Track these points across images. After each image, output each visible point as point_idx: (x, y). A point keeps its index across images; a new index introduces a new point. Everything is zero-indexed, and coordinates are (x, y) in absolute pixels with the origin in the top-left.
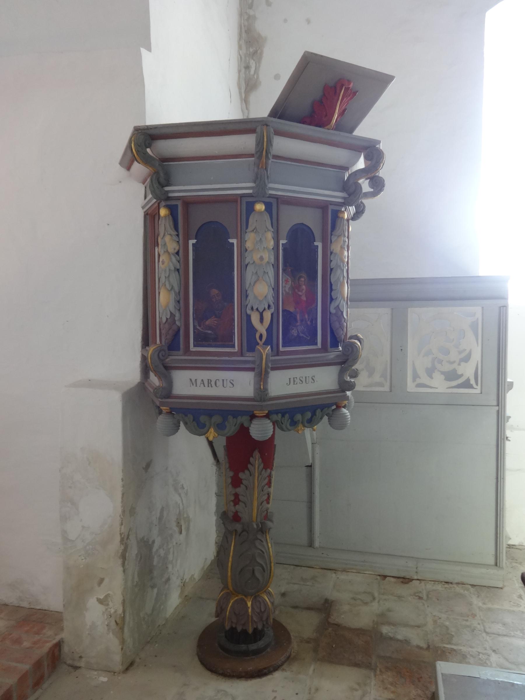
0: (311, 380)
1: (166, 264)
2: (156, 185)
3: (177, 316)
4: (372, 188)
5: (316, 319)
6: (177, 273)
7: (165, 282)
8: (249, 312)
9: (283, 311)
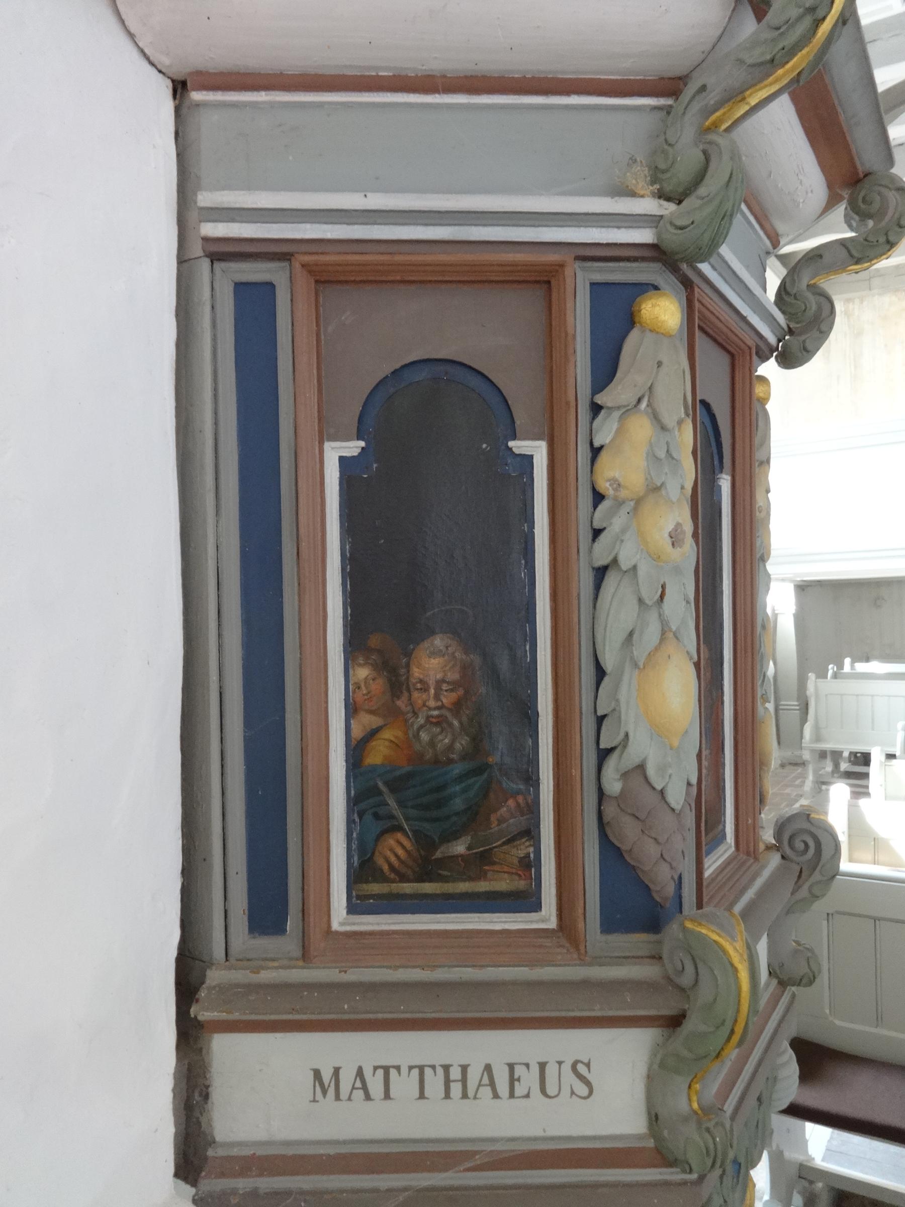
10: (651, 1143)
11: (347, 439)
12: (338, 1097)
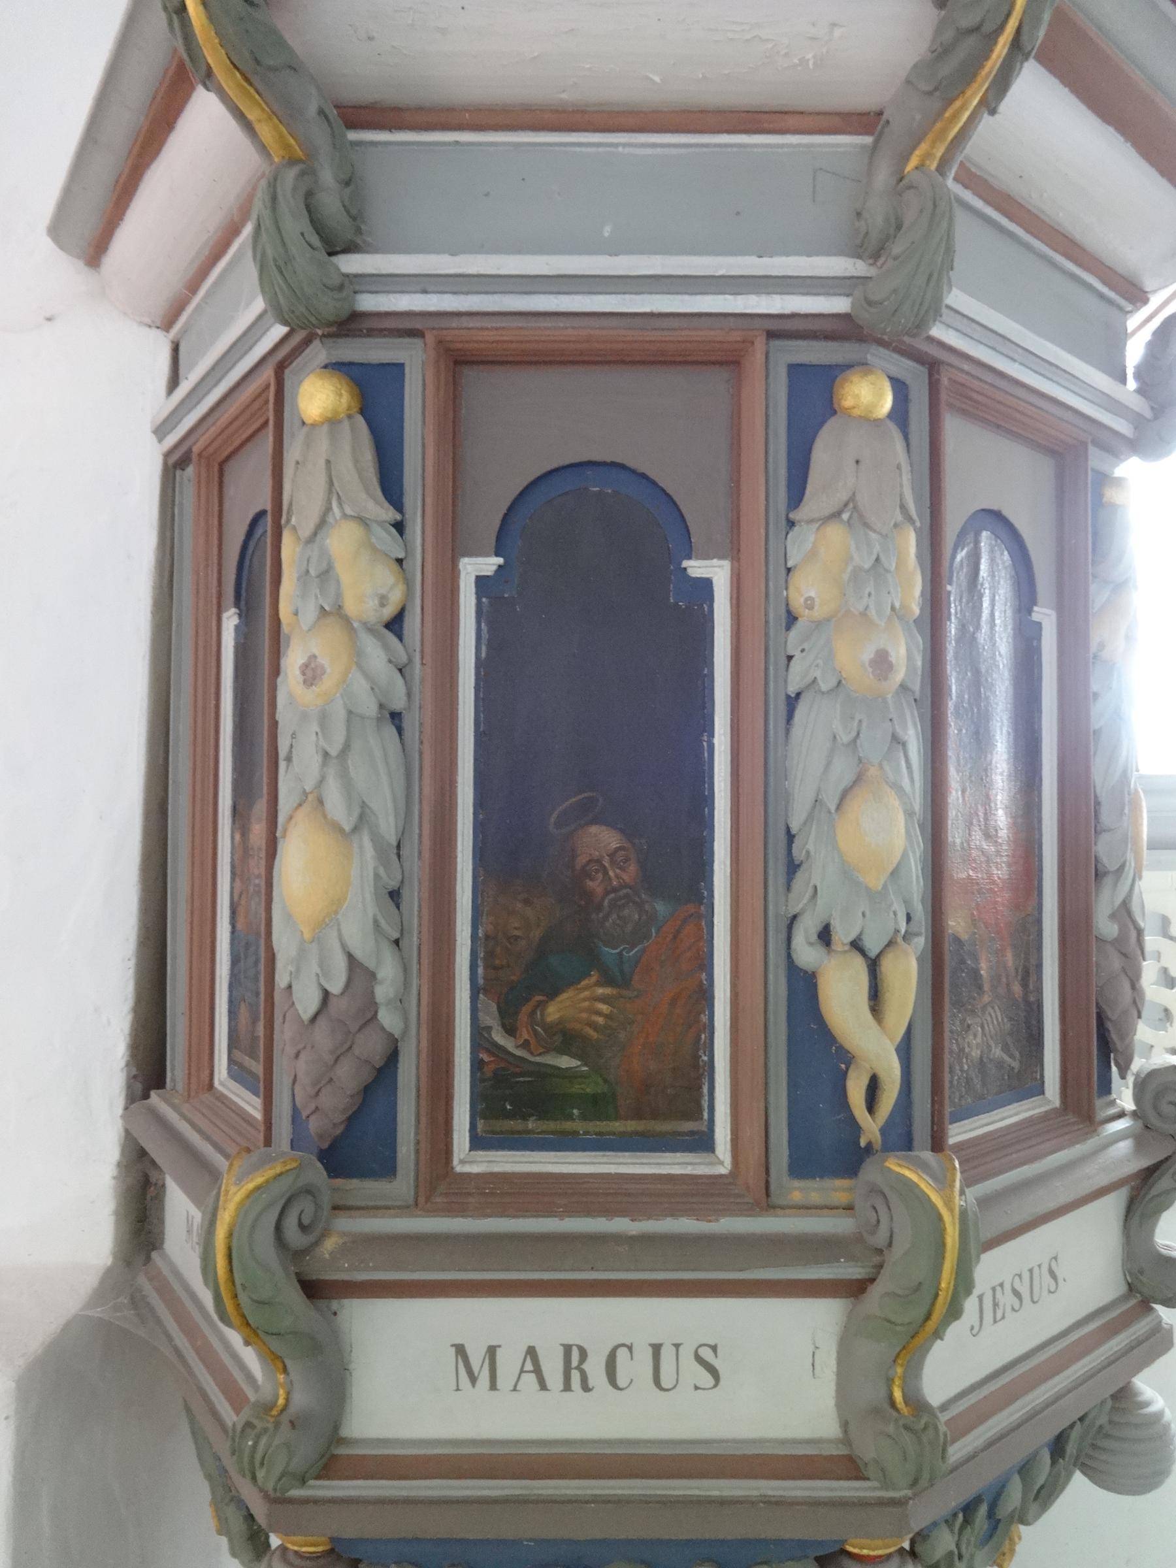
1: (328, 683)
2: (295, 225)
3: (388, 971)
6: (390, 731)
7: (322, 781)
8: (807, 954)
10: (842, 1451)
11: (487, 555)
12: (493, 1386)
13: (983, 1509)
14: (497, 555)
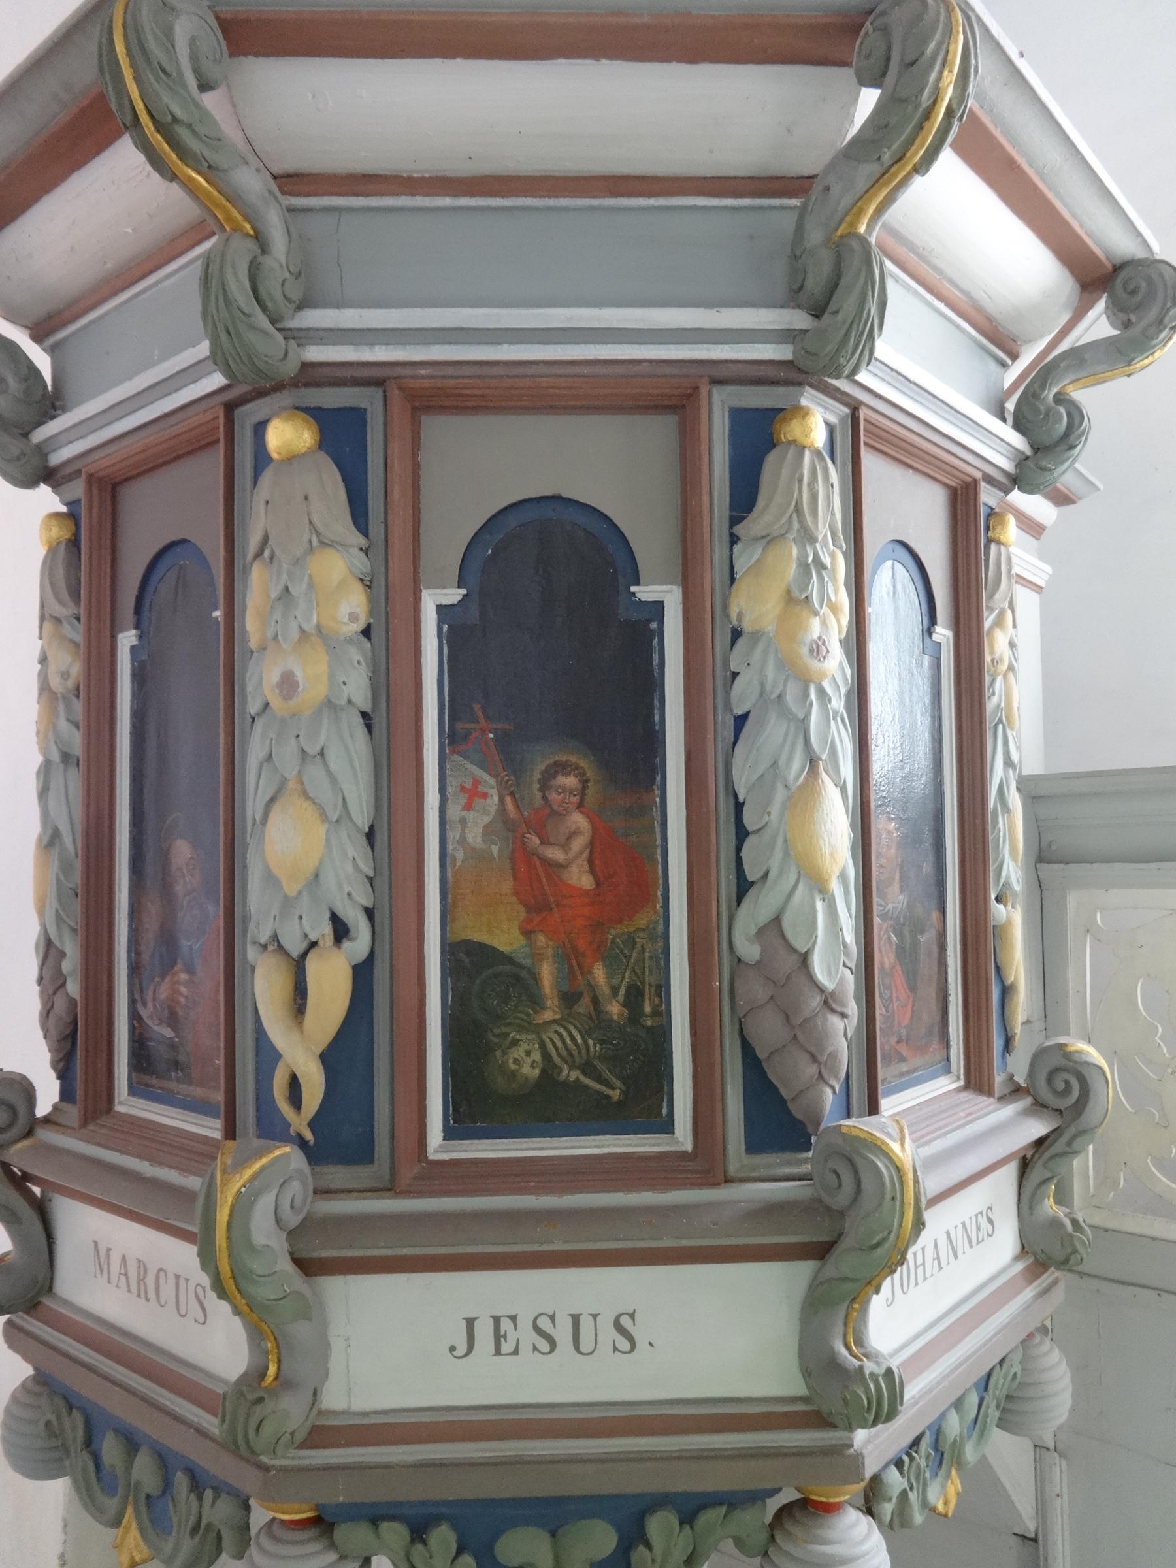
0: (608, 1333)
4: (1115, 328)
5: (663, 990)
9: (453, 951)
13: (924, 1445)
14: (459, 587)
